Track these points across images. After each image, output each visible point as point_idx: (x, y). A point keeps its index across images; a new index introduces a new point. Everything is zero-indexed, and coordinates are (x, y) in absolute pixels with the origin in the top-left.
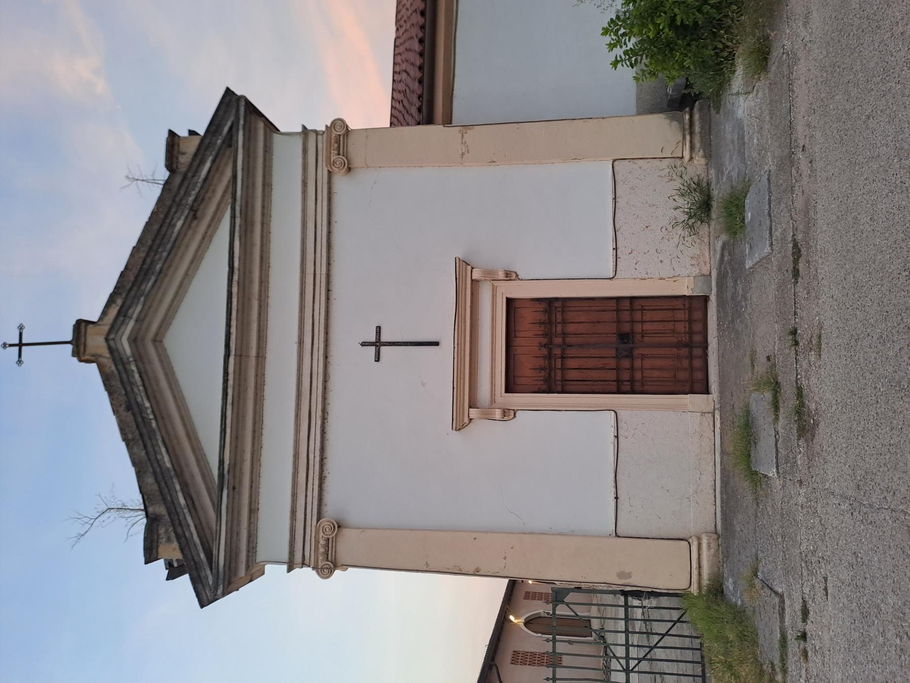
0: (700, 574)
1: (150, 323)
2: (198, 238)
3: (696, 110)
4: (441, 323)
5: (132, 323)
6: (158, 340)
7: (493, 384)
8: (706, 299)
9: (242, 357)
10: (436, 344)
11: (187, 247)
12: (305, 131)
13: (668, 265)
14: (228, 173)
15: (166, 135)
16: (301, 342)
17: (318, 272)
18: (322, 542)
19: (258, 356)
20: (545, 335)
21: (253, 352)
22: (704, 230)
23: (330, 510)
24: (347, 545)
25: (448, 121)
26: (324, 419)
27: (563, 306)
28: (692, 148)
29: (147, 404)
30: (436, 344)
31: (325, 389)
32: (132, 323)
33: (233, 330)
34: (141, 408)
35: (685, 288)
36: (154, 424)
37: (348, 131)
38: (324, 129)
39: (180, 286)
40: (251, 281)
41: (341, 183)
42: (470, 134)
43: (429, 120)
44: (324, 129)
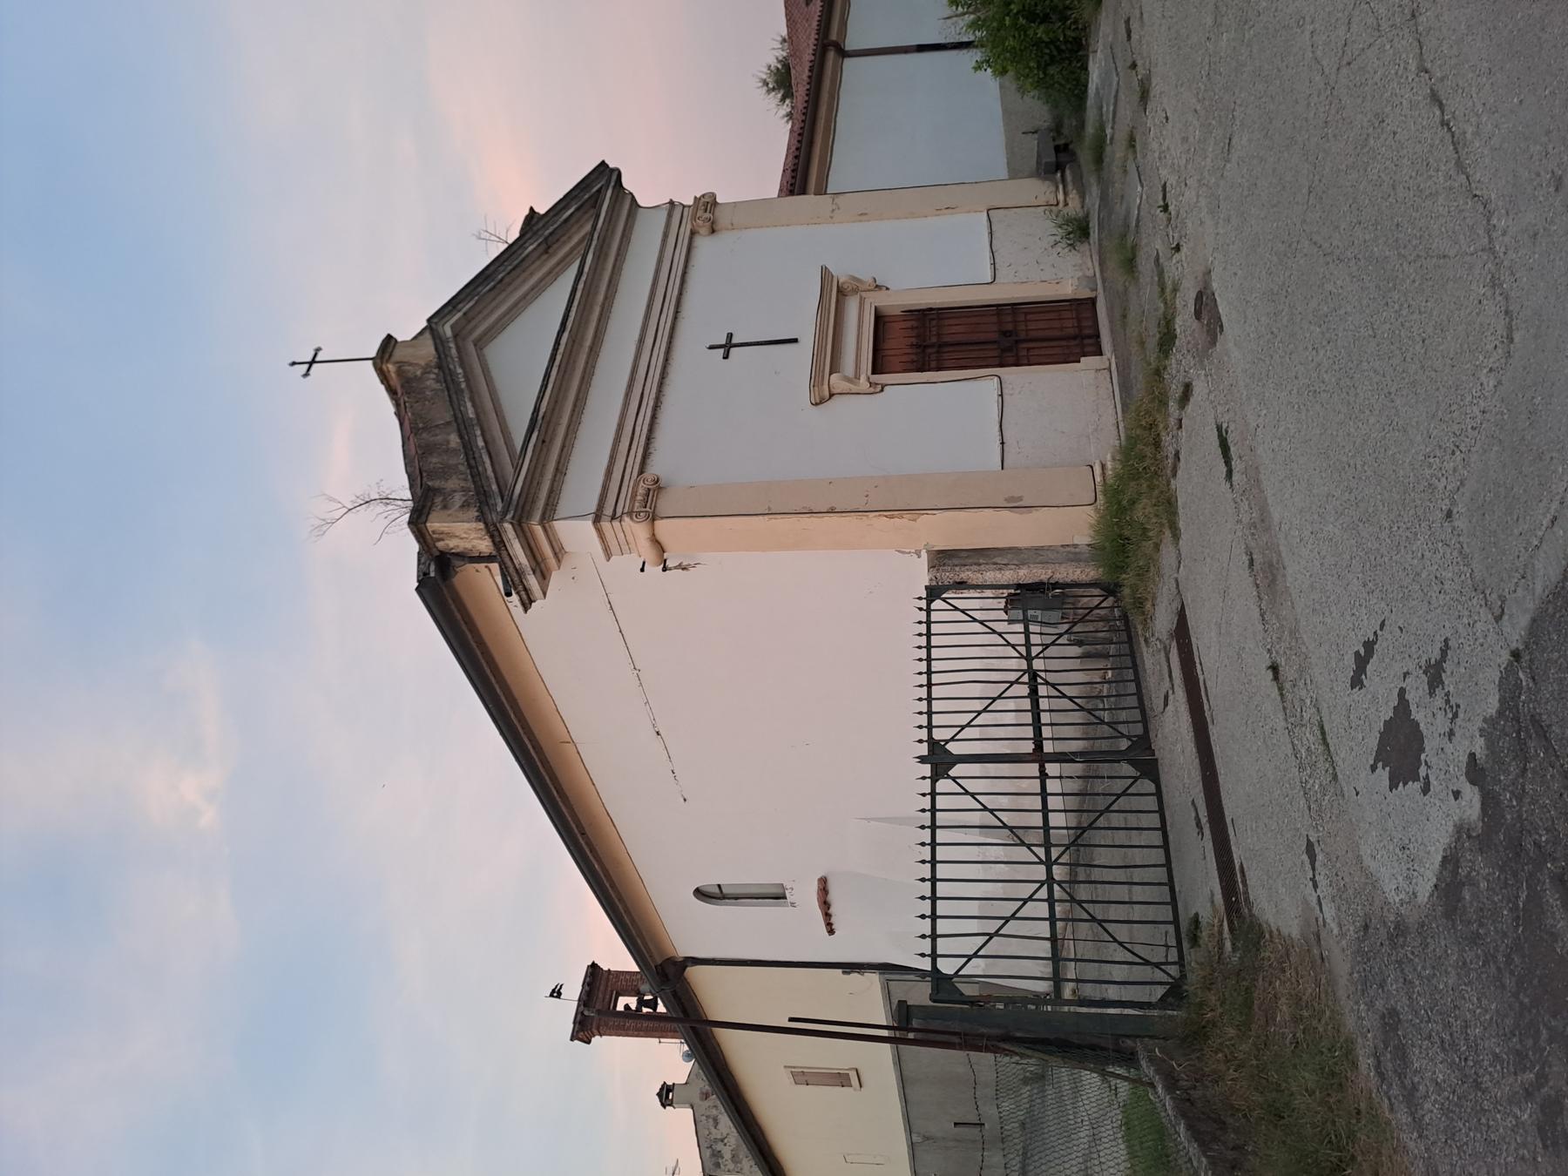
0: (1103, 474)
1: (476, 327)
2: (545, 270)
3: (1068, 172)
4: (805, 326)
5: (459, 315)
6: (480, 344)
7: (859, 349)
8: (1093, 301)
9: (575, 341)
10: (795, 341)
11: (532, 274)
12: (671, 203)
13: (1047, 272)
14: (588, 227)
15: (527, 212)
16: (641, 341)
17: (638, 429)
18: (641, 491)
19: (591, 349)
20: (917, 336)
21: (588, 343)
22: (1084, 247)
23: (657, 467)
24: (665, 504)
25: (821, 190)
26: (656, 407)
27: (908, 1020)
28: (1066, 194)
29: (460, 371)
30: (795, 341)
31: (666, 360)
32: (459, 315)
33: (572, 314)
34: (452, 373)
35: (1068, 289)
36: (463, 386)
37: (715, 203)
38: (691, 202)
39: (516, 304)
40: (596, 293)
41: (704, 244)
42: (839, 200)
43: (803, 192)
44: (691, 202)
